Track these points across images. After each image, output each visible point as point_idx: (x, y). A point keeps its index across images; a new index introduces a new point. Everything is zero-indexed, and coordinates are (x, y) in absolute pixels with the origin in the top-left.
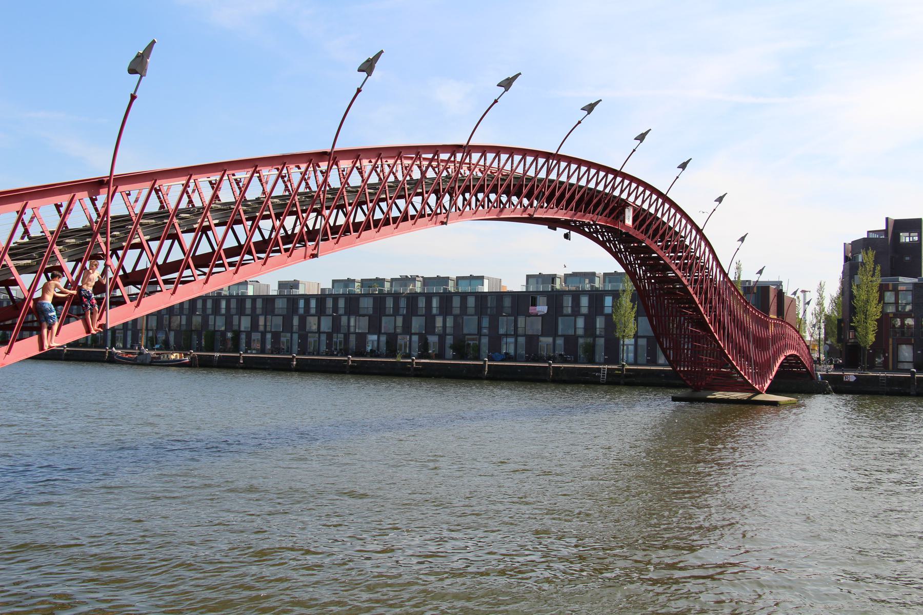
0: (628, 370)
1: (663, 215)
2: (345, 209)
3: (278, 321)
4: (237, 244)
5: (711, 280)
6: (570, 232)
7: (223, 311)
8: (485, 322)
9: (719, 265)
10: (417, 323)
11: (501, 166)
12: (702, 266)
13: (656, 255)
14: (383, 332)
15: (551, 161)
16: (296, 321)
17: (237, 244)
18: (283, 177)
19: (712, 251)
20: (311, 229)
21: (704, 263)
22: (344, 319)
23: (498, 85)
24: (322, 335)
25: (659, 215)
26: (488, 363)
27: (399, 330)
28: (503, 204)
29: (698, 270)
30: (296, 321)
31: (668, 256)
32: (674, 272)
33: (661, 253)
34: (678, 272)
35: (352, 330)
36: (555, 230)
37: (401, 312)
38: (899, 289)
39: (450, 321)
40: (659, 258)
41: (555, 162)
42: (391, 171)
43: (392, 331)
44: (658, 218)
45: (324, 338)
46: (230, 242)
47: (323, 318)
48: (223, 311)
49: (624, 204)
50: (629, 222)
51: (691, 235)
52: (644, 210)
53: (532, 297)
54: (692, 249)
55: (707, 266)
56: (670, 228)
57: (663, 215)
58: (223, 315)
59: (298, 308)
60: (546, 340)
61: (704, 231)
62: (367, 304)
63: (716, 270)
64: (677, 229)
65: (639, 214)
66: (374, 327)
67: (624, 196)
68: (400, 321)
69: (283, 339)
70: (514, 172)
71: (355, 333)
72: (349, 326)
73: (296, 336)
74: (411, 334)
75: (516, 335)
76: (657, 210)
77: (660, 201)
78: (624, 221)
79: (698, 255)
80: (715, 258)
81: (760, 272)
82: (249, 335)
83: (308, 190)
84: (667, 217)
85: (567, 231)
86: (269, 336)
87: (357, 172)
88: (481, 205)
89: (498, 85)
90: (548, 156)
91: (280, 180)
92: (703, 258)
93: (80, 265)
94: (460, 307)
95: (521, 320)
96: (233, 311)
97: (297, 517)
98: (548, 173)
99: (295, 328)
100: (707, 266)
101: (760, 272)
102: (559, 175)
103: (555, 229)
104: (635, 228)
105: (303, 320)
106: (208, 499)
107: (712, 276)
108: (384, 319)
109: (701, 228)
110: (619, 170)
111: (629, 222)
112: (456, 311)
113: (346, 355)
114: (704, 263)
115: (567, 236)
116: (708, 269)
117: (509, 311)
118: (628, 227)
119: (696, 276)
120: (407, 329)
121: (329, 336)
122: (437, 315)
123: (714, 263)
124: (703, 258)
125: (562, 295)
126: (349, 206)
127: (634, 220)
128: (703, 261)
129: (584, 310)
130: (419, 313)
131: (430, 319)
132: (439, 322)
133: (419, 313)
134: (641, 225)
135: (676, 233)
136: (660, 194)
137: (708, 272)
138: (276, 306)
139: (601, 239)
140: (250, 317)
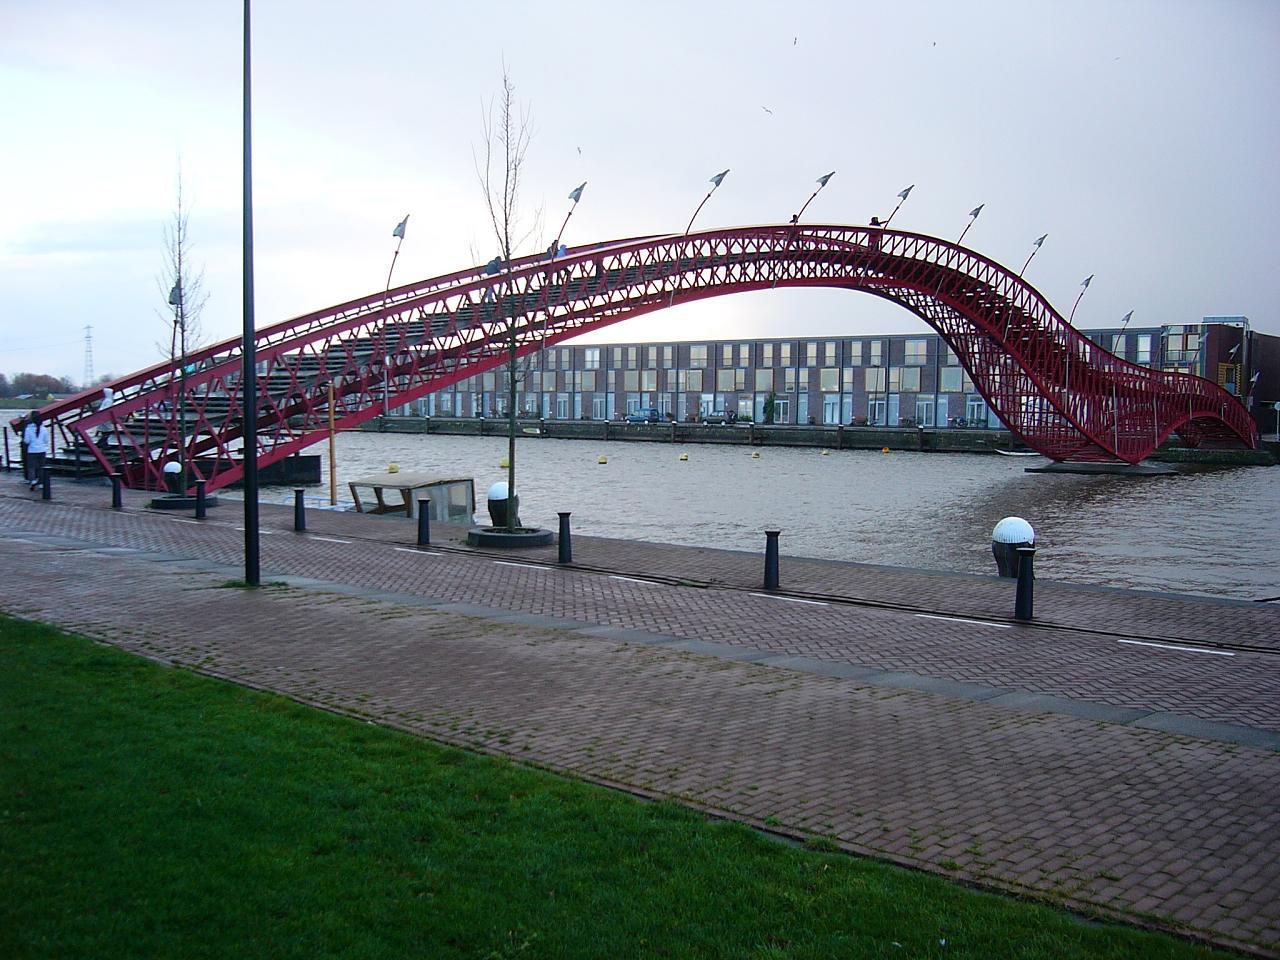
8: (848, 375)
10: (764, 380)
14: (942, 390)
16: (612, 374)
22: (672, 373)
24: (644, 395)
35: (681, 388)
37: (742, 365)
38: (180, 354)
39: (804, 374)
45: (646, 398)
47: (645, 374)
60: (708, 397)
62: (699, 355)
66: (710, 383)
68: (741, 374)
69: (597, 400)
73: (611, 397)
81: (1128, 318)
82: (554, 395)
86: (578, 398)
94: (817, 357)
95: (894, 373)
96: (565, 366)
97: (933, 718)
101: (1128, 318)
105: (619, 375)
108: (721, 373)
112: (812, 362)
121: (653, 396)
129: (745, 363)
130: (765, 365)
131: (779, 373)
132: (790, 374)
133: (765, 365)
138: (741, 356)
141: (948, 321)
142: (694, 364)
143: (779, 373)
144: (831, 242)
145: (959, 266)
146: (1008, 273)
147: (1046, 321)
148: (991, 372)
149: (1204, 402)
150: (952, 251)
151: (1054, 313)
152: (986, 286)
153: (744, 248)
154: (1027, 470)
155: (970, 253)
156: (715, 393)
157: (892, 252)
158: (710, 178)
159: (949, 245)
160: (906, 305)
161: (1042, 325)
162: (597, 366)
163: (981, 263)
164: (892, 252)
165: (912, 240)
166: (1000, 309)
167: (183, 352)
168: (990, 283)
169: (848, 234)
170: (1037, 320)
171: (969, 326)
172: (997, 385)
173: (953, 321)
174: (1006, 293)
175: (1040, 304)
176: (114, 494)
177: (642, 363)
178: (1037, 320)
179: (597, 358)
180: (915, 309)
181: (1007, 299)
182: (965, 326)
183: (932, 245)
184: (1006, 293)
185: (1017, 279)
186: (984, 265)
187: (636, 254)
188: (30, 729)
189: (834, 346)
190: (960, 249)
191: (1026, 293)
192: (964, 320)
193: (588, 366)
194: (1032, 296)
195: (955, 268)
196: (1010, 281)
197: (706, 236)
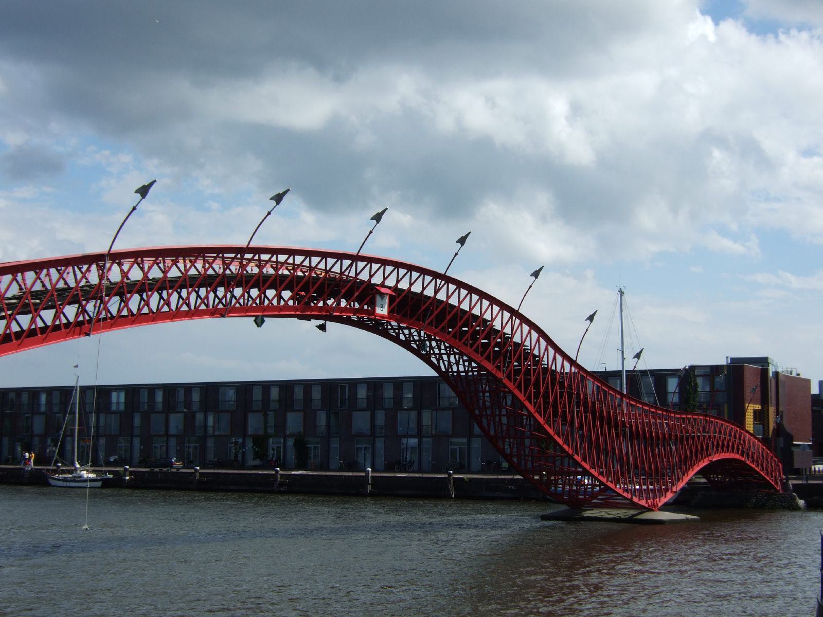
0: (281, 475)
3: (114, 421)
6: (325, 323)
7: (43, 409)
16: (137, 421)
22: (200, 416)
23: (371, 219)
26: (371, 474)
27: (270, 431)
28: (284, 300)
30: (137, 421)
35: (210, 430)
43: (261, 432)
45: (173, 442)
48: (43, 409)
53: (341, 386)
58: (43, 413)
59: (39, 404)
61: (578, 362)
71: (214, 436)
72: (206, 426)
73: (137, 441)
74: (285, 437)
75: (419, 435)
81: (638, 356)
83: (66, 287)
85: (321, 322)
86: (102, 441)
88: (184, 303)
89: (371, 219)
94: (163, 402)
99: (137, 431)
103: (310, 320)
109: (574, 359)
110: (443, 273)
113: (273, 468)
114: (530, 350)
115: (322, 328)
117: (364, 405)
120: (281, 427)
122: (319, 410)
125: (270, 385)
128: (546, 363)
140: (302, 413)
141: (445, 357)
142: (444, 403)
143: (189, 419)
144: (278, 266)
145: (424, 289)
146: (503, 307)
147: (548, 357)
148: (498, 413)
149: (720, 449)
150: (439, 281)
151: (558, 350)
152: (480, 320)
153: (165, 272)
154: (544, 518)
155: (460, 285)
156: (285, 437)
157: (370, 280)
158: (135, 190)
159: (435, 275)
160: (396, 340)
161: (546, 363)
162: (122, 407)
163: (484, 301)
164: (370, 280)
165: (377, 266)
166: (497, 344)
167: (672, 400)
168: (485, 317)
169: (315, 260)
170: (539, 356)
171: (470, 364)
172: (504, 428)
173: (452, 357)
174: (503, 328)
175: (542, 340)
176: (764, 428)
177: (170, 406)
178: (539, 356)
179: (122, 399)
180: (406, 345)
181: (505, 334)
182: (466, 364)
183: (402, 271)
184: (503, 328)
185: (514, 313)
186: (466, 292)
187: (43, 276)
188: (407, 569)
189: (320, 388)
190: (449, 280)
191: (526, 328)
192: (465, 358)
193: (114, 408)
194: (533, 331)
195: (444, 299)
196: (507, 315)
197: (138, 256)
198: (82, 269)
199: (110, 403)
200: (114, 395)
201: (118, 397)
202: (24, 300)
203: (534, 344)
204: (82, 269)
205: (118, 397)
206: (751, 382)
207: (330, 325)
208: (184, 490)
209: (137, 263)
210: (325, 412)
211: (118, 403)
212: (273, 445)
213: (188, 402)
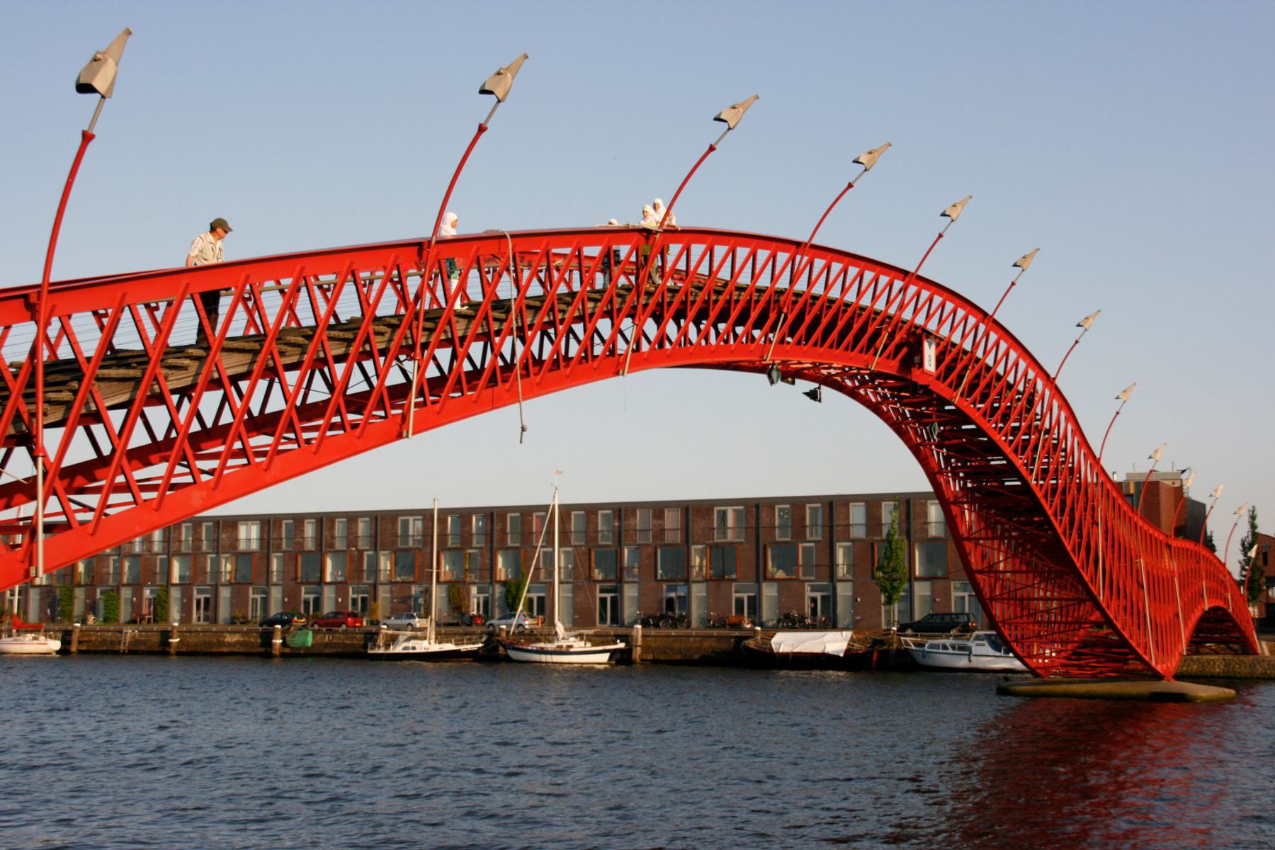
1: (986, 353)
2: (326, 370)
4: (93, 456)
5: (1071, 470)
6: (819, 388)
9: (1084, 442)
11: (692, 268)
12: (1056, 446)
13: (973, 427)
15: (798, 257)
17: (93, 456)
18: (245, 301)
19: (1072, 417)
20: (209, 424)
21: (1058, 439)
25: (980, 354)
29: (1048, 453)
31: (995, 428)
32: (1006, 458)
33: (983, 423)
34: (1012, 457)
36: (793, 383)
40: (980, 431)
41: (806, 258)
42: (562, 279)
44: (978, 360)
46: (139, 438)
49: (917, 336)
50: (930, 364)
51: (1051, 414)
52: (954, 345)
54: (1037, 414)
55: (1063, 446)
56: (999, 378)
57: (986, 353)
61: (1058, 382)
63: (1072, 441)
64: (1011, 379)
65: (945, 349)
67: (920, 320)
70: (715, 277)
76: (975, 345)
77: (982, 327)
78: (921, 364)
79: (1047, 425)
80: (1078, 430)
84: (993, 356)
85: (813, 386)
87: (538, 283)
90: (796, 246)
91: (240, 307)
92: (1056, 431)
93: (298, 403)
98: (793, 281)
100: (1063, 446)
102: (810, 284)
104: (938, 378)
106: (323, 801)
107: (1073, 463)
109: (1052, 375)
111: (930, 364)
115: (813, 395)
116: (1065, 450)
118: (928, 374)
119: (1044, 464)
123: (1076, 440)
124: (1056, 431)
126: (381, 355)
127: (939, 360)
128: (1055, 436)
134: (949, 370)
135: (1010, 387)
136: (983, 315)
137: (1065, 457)
139: (874, 400)
161: (1055, 436)
198: (156, 313)
199: (237, 540)
200: (243, 531)
201: (248, 532)
202: (371, 411)
203: (836, 285)
204: (156, 313)
205: (248, 532)
206: (1165, 501)
207: (826, 392)
208: (31, 632)
209: (391, 281)
210: (943, 535)
211: (249, 540)
212: (255, 596)
213: (352, 538)
